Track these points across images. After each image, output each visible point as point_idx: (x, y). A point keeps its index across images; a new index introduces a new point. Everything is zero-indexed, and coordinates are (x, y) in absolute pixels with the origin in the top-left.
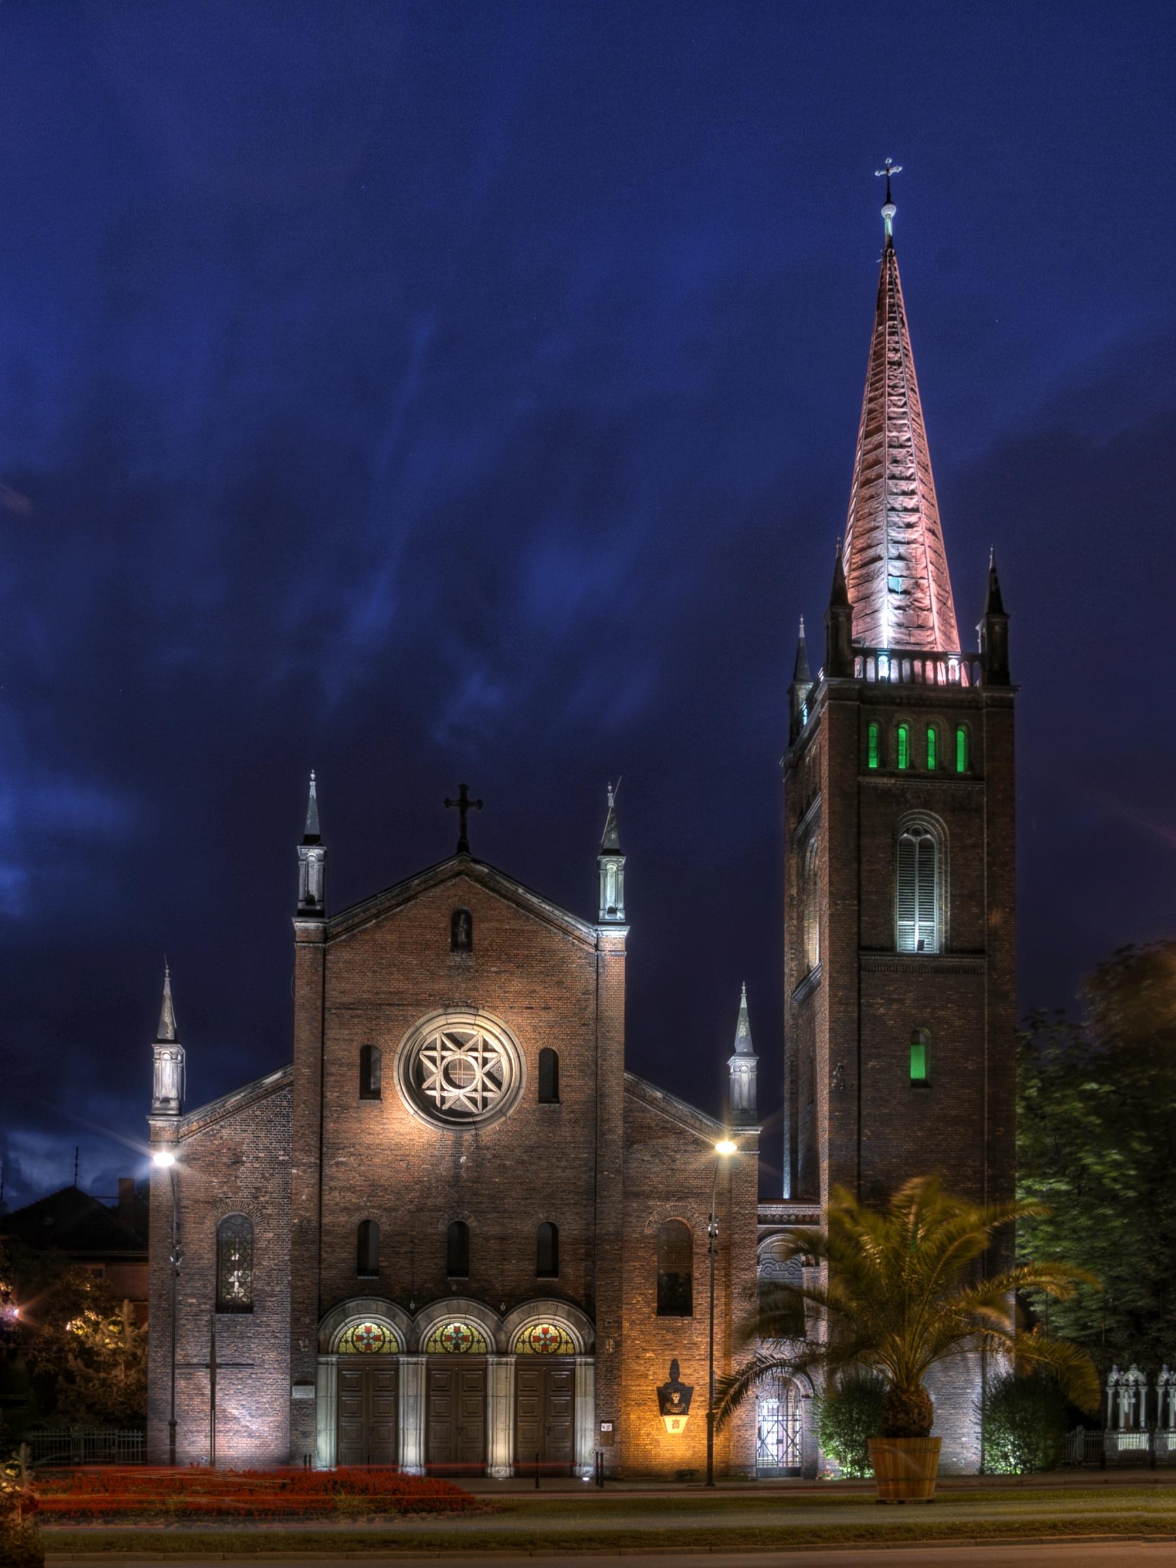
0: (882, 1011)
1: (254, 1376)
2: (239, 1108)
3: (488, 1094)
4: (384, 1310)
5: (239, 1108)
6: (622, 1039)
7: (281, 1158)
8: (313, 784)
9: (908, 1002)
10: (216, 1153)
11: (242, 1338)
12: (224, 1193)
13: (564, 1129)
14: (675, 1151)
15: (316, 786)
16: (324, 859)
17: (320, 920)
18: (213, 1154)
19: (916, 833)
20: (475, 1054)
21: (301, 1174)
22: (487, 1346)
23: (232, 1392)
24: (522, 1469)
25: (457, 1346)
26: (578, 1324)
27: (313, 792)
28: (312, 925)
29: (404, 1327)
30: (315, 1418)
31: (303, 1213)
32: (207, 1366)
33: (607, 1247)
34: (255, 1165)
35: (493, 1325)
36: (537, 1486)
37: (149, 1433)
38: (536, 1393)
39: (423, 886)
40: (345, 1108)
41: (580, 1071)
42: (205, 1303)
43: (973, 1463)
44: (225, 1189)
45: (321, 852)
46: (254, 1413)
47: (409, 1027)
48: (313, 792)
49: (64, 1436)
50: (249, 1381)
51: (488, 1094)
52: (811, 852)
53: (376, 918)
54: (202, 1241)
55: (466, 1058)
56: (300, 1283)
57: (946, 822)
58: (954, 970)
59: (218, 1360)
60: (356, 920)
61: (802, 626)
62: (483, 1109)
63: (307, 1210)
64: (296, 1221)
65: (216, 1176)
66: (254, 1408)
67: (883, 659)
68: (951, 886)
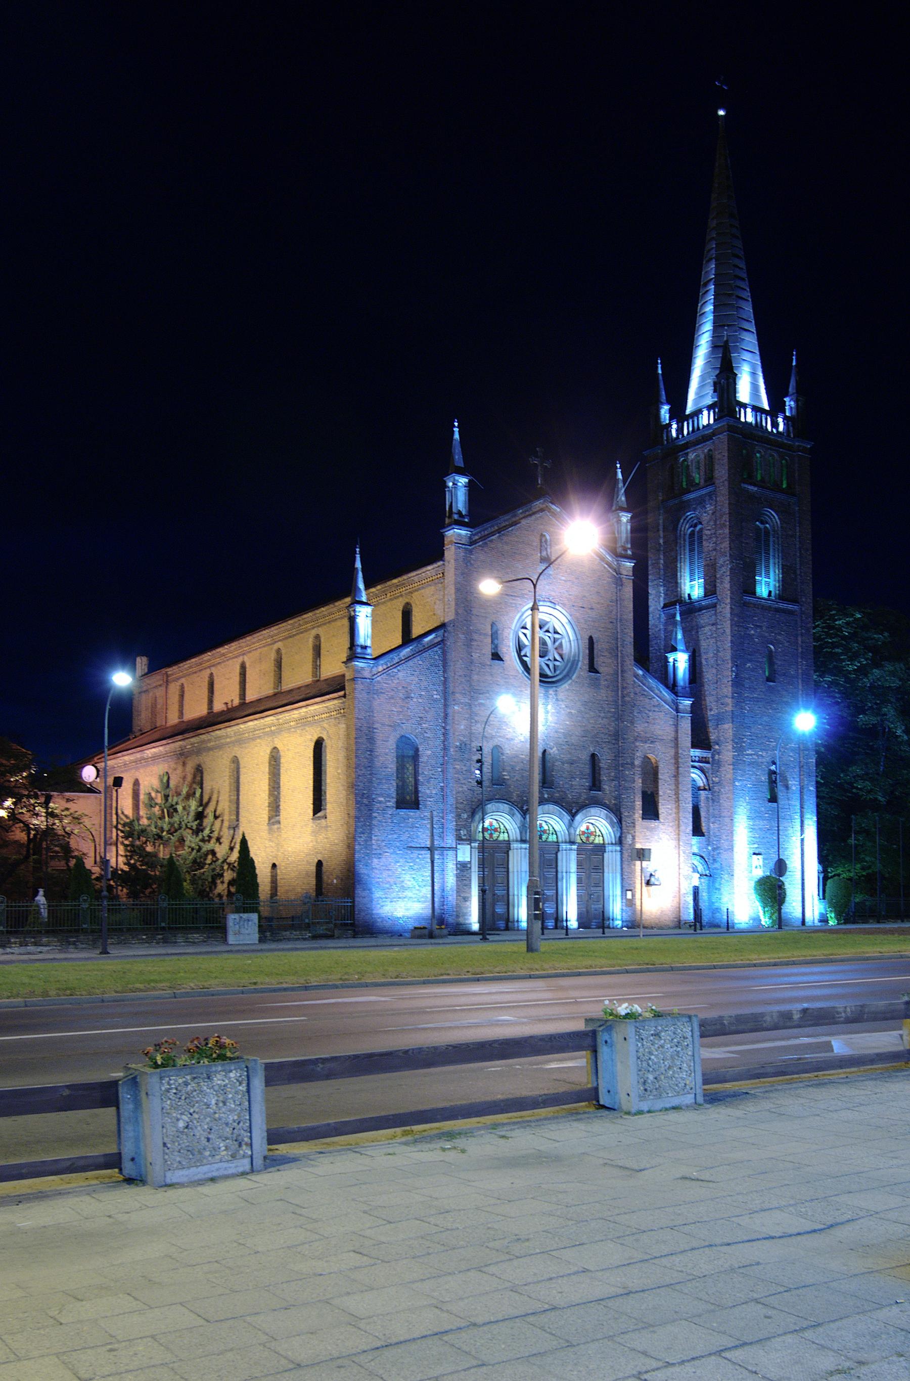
0: (752, 632)
1: (420, 856)
2: (408, 658)
3: (557, 663)
4: (508, 809)
5: (408, 658)
6: (632, 635)
7: (435, 696)
8: (456, 430)
9: (764, 628)
10: (396, 690)
11: (413, 827)
12: (401, 719)
13: (602, 691)
14: (649, 711)
15: (459, 431)
16: (470, 486)
17: (469, 529)
18: (393, 690)
19: (762, 523)
20: (549, 634)
21: (461, 710)
22: (508, 836)
23: (407, 868)
24: (583, 922)
25: (588, 838)
26: (612, 824)
27: (457, 436)
28: (464, 532)
29: (518, 822)
30: (470, 888)
31: (462, 738)
32: (429, 849)
33: (627, 773)
34: (420, 701)
35: (567, 821)
36: (604, 933)
37: (357, 899)
38: (584, 871)
39: (523, 515)
40: (483, 665)
41: (610, 653)
42: (389, 801)
43: (798, 918)
44: (401, 717)
45: (467, 480)
46: (420, 884)
47: (519, 612)
48: (457, 436)
49: (151, 905)
50: (418, 860)
51: (557, 663)
52: (685, 519)
53: (499, 533)
54: (387, 755)
55: (544, 637)
56: (461, 789)
57: (779, 519)
58: (777, 610)
59: (428, 844)
60: (486, 532)
61: (660, 366)
62: (555, 672)
63: (464, 736)
64: (458, 744)
65: (395, 706)
66: (420, 880)
67: (749, 410)
68: (782, 559)
